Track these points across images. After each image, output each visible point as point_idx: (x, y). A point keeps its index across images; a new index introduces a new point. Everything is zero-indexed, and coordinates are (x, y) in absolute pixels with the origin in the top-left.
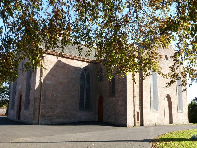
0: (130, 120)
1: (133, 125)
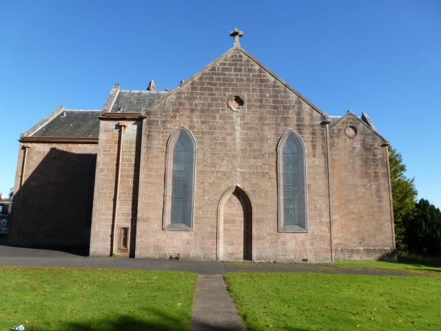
0: (100, 241)
1: (109, 253)
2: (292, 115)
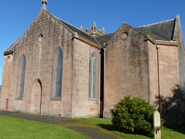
2: (60, 38)
